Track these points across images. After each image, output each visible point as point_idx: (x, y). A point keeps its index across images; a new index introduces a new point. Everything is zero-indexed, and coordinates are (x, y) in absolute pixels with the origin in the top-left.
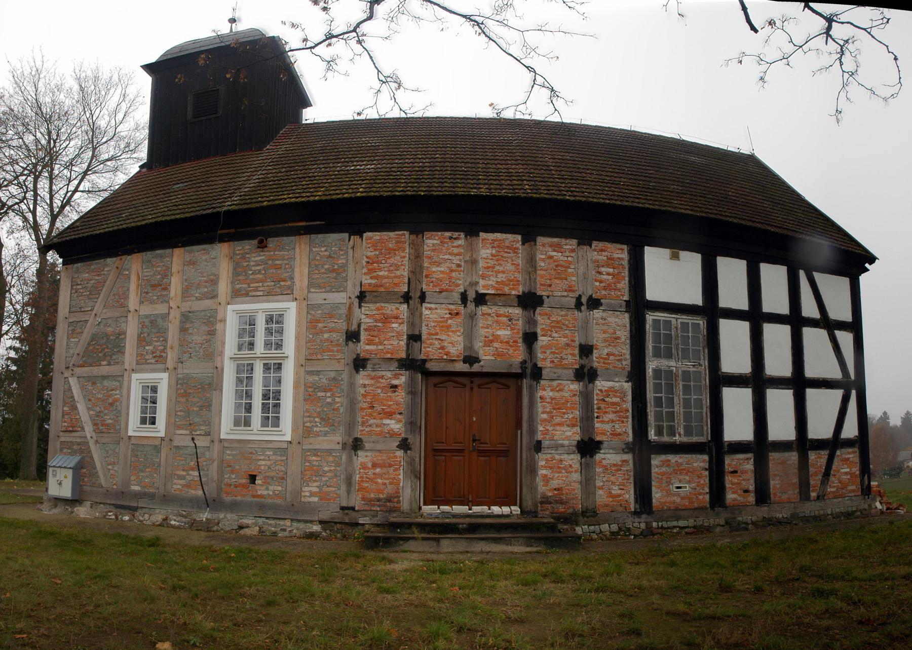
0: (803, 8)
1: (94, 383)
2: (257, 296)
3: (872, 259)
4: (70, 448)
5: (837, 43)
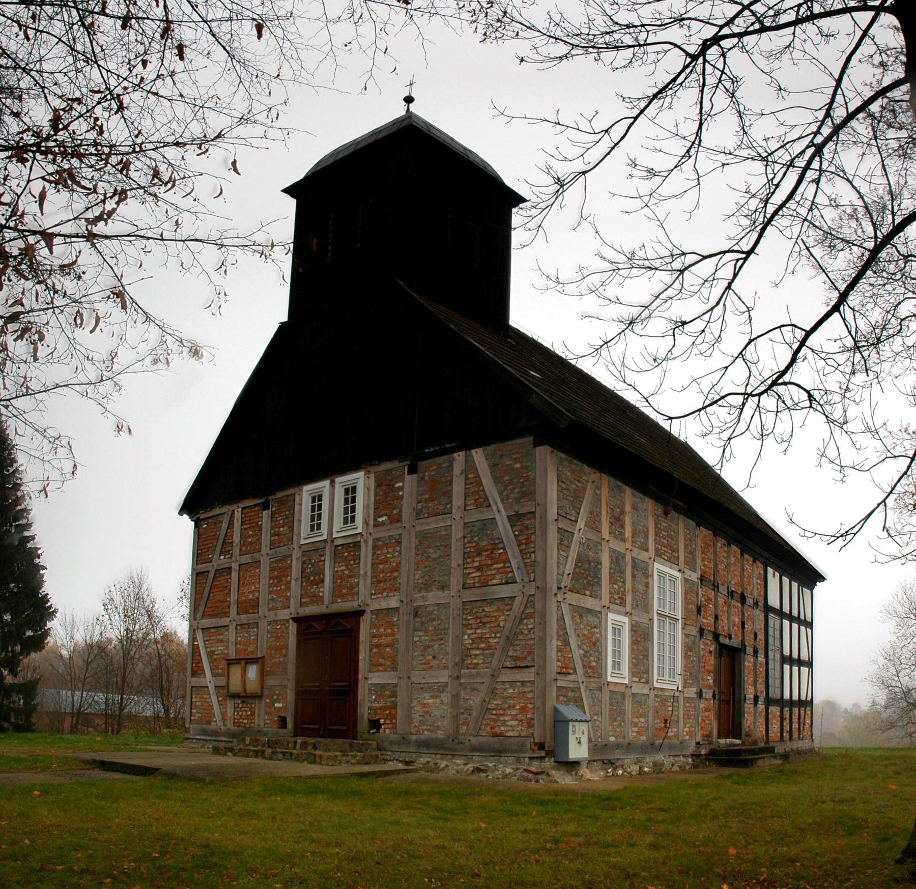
0: (814, 700)
1: (581, 616)
2: (172, 776)
3: (822, 578)
4: (566, 696)
5: (723, 293)
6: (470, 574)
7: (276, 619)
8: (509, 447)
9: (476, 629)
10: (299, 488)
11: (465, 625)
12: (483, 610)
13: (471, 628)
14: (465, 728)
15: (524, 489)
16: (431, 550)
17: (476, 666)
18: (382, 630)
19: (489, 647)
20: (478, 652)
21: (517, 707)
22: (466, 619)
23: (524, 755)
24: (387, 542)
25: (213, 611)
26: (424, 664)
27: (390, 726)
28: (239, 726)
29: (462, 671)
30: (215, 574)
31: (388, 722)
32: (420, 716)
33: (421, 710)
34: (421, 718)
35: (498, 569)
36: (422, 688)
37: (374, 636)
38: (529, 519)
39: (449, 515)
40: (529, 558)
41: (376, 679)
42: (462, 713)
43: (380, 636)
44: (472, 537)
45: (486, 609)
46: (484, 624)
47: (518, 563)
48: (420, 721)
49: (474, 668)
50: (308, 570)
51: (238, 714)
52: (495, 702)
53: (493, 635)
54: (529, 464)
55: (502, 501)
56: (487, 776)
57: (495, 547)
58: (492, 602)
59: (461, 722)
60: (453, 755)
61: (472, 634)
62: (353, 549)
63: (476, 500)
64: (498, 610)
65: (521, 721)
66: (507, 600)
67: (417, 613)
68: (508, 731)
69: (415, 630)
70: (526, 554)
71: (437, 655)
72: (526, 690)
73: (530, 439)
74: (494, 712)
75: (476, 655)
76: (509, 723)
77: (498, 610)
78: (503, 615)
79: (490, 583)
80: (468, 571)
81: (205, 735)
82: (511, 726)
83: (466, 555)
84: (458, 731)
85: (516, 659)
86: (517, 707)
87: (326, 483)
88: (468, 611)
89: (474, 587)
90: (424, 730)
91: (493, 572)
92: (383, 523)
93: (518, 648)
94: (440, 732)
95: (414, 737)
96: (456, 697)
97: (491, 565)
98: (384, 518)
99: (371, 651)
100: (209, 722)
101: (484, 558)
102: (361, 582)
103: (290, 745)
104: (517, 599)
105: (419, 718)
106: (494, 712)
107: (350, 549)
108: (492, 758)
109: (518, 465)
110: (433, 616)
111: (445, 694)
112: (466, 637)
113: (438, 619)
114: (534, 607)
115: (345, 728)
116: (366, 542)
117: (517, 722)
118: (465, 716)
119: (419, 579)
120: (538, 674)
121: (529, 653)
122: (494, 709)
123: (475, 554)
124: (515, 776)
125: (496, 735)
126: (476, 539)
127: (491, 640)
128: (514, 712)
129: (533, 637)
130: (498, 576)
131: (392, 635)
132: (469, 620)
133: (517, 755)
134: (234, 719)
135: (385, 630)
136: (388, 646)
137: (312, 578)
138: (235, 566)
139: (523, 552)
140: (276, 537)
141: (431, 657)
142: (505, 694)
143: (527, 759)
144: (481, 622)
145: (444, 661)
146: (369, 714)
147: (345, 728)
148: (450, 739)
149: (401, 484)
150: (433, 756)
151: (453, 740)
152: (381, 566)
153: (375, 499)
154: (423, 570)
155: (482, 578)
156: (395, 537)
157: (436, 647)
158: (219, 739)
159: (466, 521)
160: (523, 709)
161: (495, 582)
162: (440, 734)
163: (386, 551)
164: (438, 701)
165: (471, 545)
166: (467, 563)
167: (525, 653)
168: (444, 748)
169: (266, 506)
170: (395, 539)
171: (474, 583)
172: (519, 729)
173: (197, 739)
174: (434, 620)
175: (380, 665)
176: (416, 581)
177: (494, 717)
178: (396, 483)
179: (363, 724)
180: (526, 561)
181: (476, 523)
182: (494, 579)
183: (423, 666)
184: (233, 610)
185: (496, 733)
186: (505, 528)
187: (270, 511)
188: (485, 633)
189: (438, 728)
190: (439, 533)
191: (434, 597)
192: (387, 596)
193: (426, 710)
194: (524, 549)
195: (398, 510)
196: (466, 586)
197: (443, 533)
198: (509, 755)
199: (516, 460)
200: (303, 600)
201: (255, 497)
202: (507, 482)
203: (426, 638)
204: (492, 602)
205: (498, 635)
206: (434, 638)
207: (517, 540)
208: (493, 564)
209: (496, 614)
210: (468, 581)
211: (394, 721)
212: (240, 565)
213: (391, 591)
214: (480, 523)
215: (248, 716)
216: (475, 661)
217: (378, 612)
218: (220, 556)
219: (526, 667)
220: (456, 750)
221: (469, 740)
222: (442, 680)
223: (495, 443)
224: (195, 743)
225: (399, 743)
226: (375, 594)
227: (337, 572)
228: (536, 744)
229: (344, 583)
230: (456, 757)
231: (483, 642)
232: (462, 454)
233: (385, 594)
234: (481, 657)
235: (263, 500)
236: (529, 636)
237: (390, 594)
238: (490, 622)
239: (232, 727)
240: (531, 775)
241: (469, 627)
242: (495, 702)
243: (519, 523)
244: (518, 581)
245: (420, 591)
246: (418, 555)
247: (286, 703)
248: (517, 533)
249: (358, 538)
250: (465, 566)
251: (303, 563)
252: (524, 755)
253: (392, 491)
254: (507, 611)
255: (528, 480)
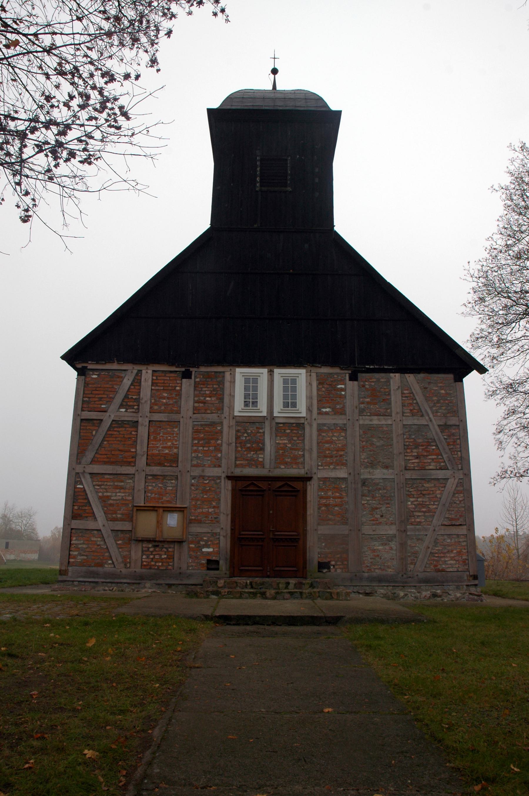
6: (409, 460)
7: (203, 474)
8: (435, 378)
9: (418, 498)
10: (231, 368)
11: (408, 495)
12: (423, 486)
13: (414, 497)
14: (412, 566)
15: (449, 408)
16: (374, 440)
17: (419, 523)
18: (330, 493)
19: (429, 511)
20: (420, 514)
21: (455, 552)
22: (408, 491)
23: (463, 584)
24: (333, 428)
25: (108, 458)
26: (373, 520)
27: (341, 567)
28: (150, 568)
29: (408, 527)
30: (111, 424)
31: (339, 563)
32: (371, 558)
33: (372, 555)
34: (372, 560)
35: (433, 459)
36: (372, 538)
37: (322, 498)
38: (454, 429)
39: (389, 417)
40: (456, 455)
41: (324, 530)
42: (409, 556)
43: (328, 498)
44: (410, 435)
45: (425, 485)
46: (423, 495)
47: (448, 457)
48: (371, 562)
49: (417, 525)
50: (244, 438)
51: (148, 558)
52: (436, 548)
53: (432, 503)
54: (451, 392)
55: (433, 413)
56: (442, 600)
57: (429, 444)
58: (429, 480)
59: (409, 562)
60: (403, 586)
61: (415, 501)
62: (295, 428)
63: (411, 410)
64: (435, 486)
65: (457, 561)
66: (441, 481)
67: (364, 483)
68: (449, 568)
69: (363, 495)
70: (454, 451)
71: (384, 515)
72: (461, 540)
73: (451, 376)
74: (436, 555)
75: (419, 516)
76: (449, 562)
77: (435, 486)
78: (440, 490)
79: (427, 468)
80: (408, 458)
81: (94, 577)
82: (450, 564)
83: (406, 447)
84: (406, 569)
85: (452, 519)
86: (455, 552)
87: (264, 371)
88: (410, 486)
89: (414, 470)
90: (375, 569)
91: (429, 461)
92: (327, 413)
93: (453, 512)
94: (390, 570)
95: (366, 575)
96: (403, 545)
97: (427, 456)
98: (328, 410)
99: (319, 509)
100: (101, 565)
101: (421, 450)
102: (307, 455)
103: (281, 586)
104: (449, 480)
105: (370, 561)
106: (436, 555)
107: (293, 428)
108: (437, 587)
109: (443, 392)
110: (379, 487)
111: (393, 543)
112: (409, 503)
113: (384, 489)
114: (463, 487)
115: (295, 569)
116: (311, 425)
117: (454, 562)
118: (412, 558)
119: (364, 459)
120: (469, 530)
121: (461, 516)
122: (436, 553)
123: (413, 447)
124: (464, 598)
125: (438, 571)
126: (413, 437)
127: (430, 506)
128: (452, 555)
129: (463, 506)
130: (433, 464)
131: (340, 498)
132: (411, 491)
133: (456, 584)
134: (142, 562)
135: (332, 493)
136: (336, 506)
137: (249, 445)
138: (144, 422)
139: (452, 450)
140: (201, 405)
141: (379, 516)
142: (445, 543)
143: (465, 586)
144: (421, 494)
145: (391, 519)
146: (319, 557)
147: (295, 569)
148: (400, 575)
149: (343, 386)
150: (385, 587)
151: (402, 575)
152: (327, 445)
153: (317, 393)
154: (369, 453)
155: (420, 464)
156: (341, 425)
157: (383, 508)
158: (116, 581)
159: (404, 423)
160: (459, 553)
161: (431, 467)
162: (390, 572)
163: (331, 435)
164: (387, 547)
165: (410, 441)
166: (407, 452)
167: (458, 516)
168: (396, 582)
169: (187, 375)
170: (340, 427)
171: (414, 467)
172: (457, 566)
173: (79, 581)
174: (380, 489)
175: (329, 520)
176: (362, 460)
177: (436, 558)
178: (338, 385)
179: (313, 565)
180: (454, 456)
181: (413, 426)
182: (430, 465)
183: (372, 522)
184: (142, 461)
185: (439, 569)
186: (437, 434)
187: (192, 381)
188: (426, 502)
189: (389, 567)
190: (381, 429)
191: (379, 474)
192: (334, 468)
193: (376, 554)
194: (452, 448)
195: (342, 406)
196: (408, 468)
197: (385, 429)
198: (450, 584)
199: (442, 388)
200: (238, 462)
201: (171, 363)
202: (435, 401)
203: (374, 502)
204: (429, 480)
205: (436, 503)
206: (381, 502)
207: (446, 442)
208: (429, 456)
209: (433, 489)
210: (409, 465)
211: (346, 562)
212: (150, 421)
213: (338, 465)
214: (416, 427)
215: (162, 559)
216: (418, 520)
217: (325, 480)
218: (120, 408)
219: (461, 525)
220: (406, 582)
221: (417, 575)
222: (391, 532)
223: (423, 373)
224: (76, 586)
225: (351, 580)
226: (321, 466)
227: (279, 443)
228: (471, 576)
229: (286, 453)
230: (405, 587)
231: (424, 507)
232: (397, 375)
233: (332, 467)
234: (423, 517)
235: (183, 369)
236: (460, 505)
237: (337, 467)
238: (429, 494)
239: (139, 570)
240: (476, 597)
241: (412, 496)
242: (436, 548)
243: (447, 431)
244: (449, 468)
245: (366, 467)
246: (363, 442)
247: (219, 547)
248: (446, 437)
249: (302, 421)
250: (406, 454)
251: (238, 431)
252: (463, 584)
253: (334, 390)
254: (442, 487)
255: (451, 402)
